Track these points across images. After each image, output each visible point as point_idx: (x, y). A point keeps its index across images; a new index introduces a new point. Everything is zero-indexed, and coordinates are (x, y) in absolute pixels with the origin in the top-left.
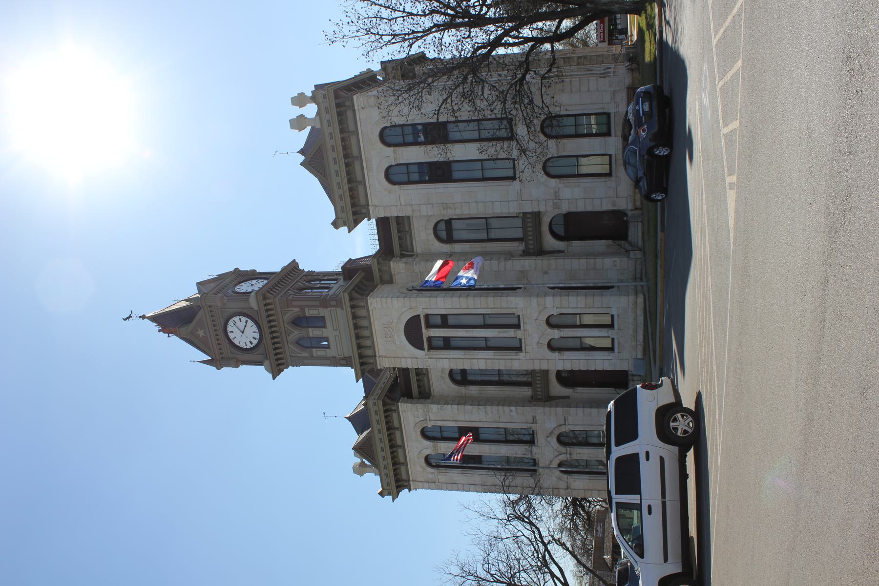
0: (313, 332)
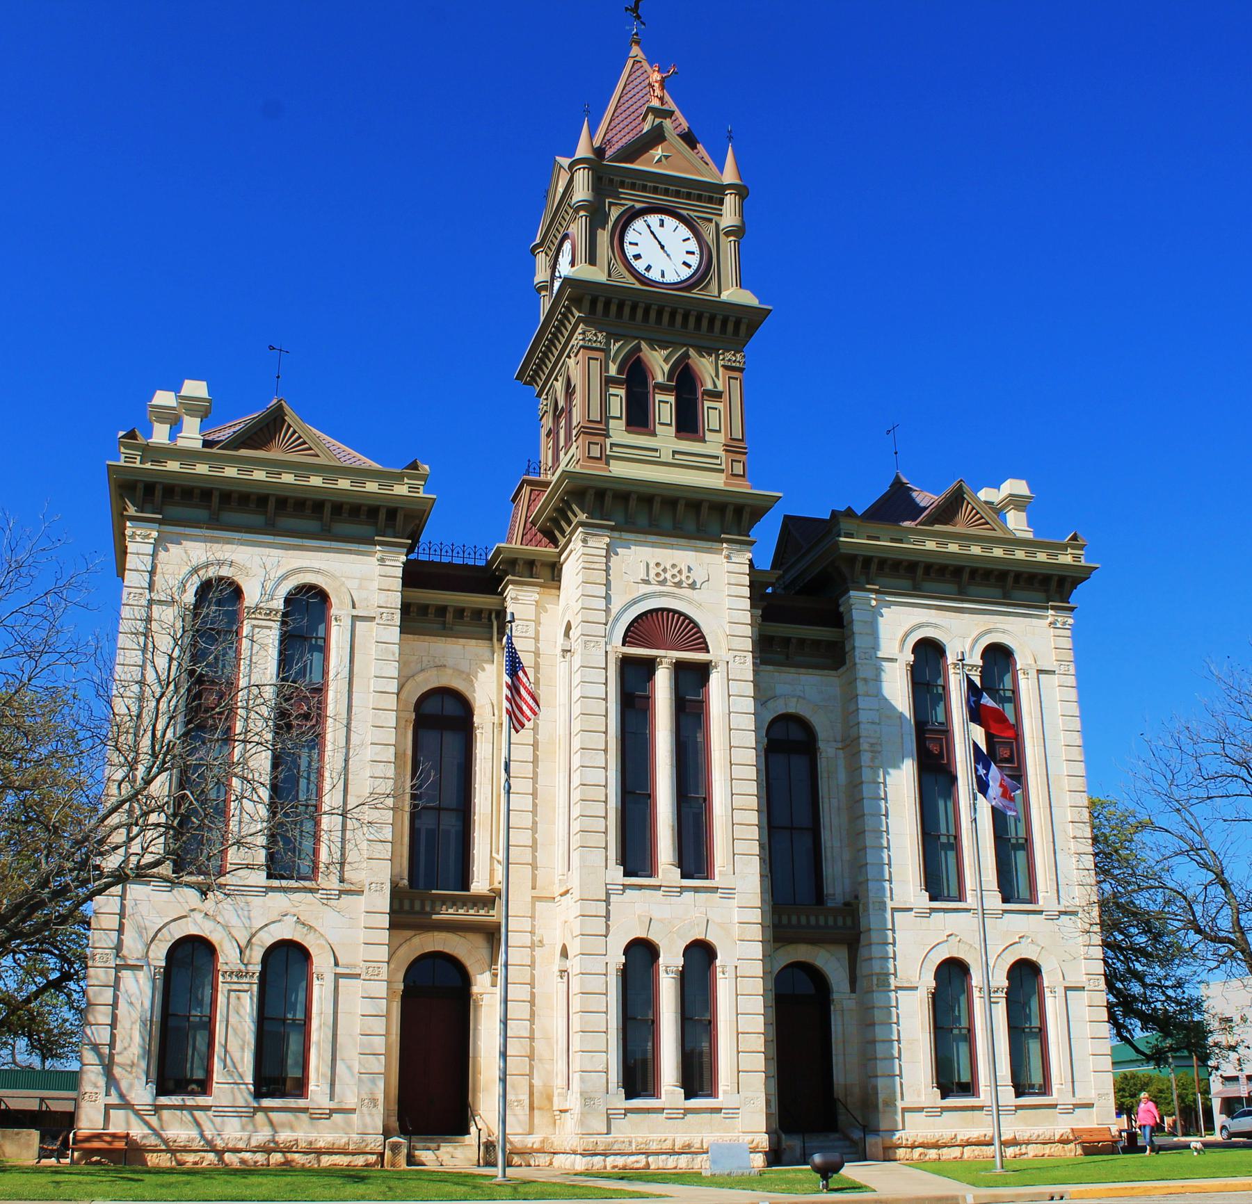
0: (664, 407)
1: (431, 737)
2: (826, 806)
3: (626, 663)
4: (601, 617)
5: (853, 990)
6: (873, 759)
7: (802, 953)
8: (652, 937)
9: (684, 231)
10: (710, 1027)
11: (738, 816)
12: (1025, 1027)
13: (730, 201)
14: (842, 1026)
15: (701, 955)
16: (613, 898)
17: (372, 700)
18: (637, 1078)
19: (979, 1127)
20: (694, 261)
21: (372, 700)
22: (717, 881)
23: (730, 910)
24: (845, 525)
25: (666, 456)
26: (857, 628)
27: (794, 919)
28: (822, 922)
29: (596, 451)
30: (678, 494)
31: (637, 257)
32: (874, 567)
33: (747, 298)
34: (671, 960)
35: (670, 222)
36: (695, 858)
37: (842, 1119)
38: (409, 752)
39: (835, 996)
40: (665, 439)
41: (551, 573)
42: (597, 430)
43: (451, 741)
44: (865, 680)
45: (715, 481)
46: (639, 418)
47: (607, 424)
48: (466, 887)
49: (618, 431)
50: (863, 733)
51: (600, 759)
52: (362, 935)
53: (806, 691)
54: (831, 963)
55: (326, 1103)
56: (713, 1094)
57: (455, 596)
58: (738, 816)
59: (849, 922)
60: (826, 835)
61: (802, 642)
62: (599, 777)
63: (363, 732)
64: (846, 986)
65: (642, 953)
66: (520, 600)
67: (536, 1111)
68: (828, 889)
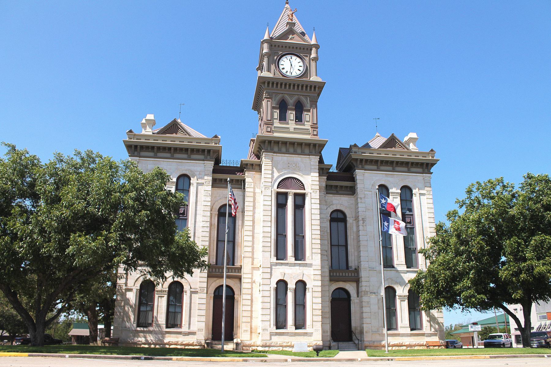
1: (334, 224)
2: (240, 234)
3: (278, 194)
4: (270, 180)
5: (358, 296)
6: (363, 223)
7: (341, 285)
8: (304, 279)
9: (298, 60)
10: (304, 306)
11: (314, 241)
12: (300, 305)
13: (314, 50)
14: (354, 308)
15: (301, 285)
16: (273, 267)
17: (203, 208)
18: (280, 324)
19: (424, 340)
20: (301, 69)
21: (203, 208)
22: (307, 261)
23: (312, 271)
24: (354, 150)
25: (292, 130)
26: (358, 181)
27: (347, 275)
28: (338, 275)
29: (269, 129)
30: (287, 140)
31: (283, 69)
32: (364, 162)
33: (319, 79)
34: (291, 285)
35: (294, 58)
36: (299, 254)
37: (354, 337)
38: (216, 224)
39: (352, 298)
40: (292, 125)
41: (258, 168)
42: (269, 123)
43: (341, 225)
44: (361, 198)
45: (308, 137)
47: (273, 121)
48: (233, 265)
49: (277, 123)
50: (360, 215)
51: (269, 224)
52: (199, 279)
53: (341, 202)
54: (350, 287)
55: (187, 330)
56: (396, 329)
57: (228, 176)
58: (314, 241)
59: (356, 275)
60: (349, 247)
61: (342, 187)
62: (268, 229)
63: (199, 218)
64: (355, 295)
65: (282, 284)
66: (249, 177)
67: (253, 334)
68: (350, 264)
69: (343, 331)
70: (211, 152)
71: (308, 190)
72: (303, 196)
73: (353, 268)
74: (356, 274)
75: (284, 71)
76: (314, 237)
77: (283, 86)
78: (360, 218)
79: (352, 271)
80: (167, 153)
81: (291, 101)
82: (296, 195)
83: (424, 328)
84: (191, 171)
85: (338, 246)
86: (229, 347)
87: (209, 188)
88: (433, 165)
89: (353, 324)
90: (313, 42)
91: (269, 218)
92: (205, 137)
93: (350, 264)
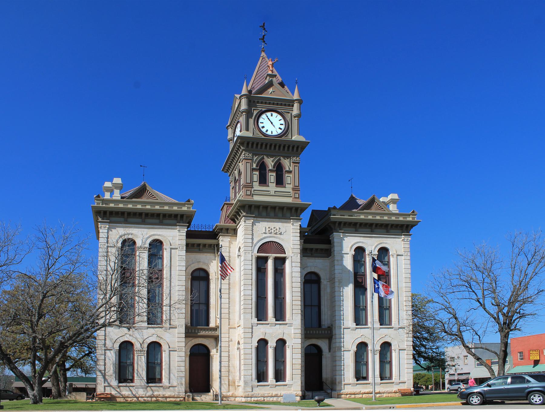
0: (272, 177)
3: (258, 258)
5: (330, 351)
8: (266, 338)
9: (280, 117)
13: (296, 105)
18: (261, 376)
20: (283, 127)
22: (287, 321)
23: (291, 330)
24: (333, 212)
26: (335, 244)
30: (276, 205)
31: (263, 127)
32: (342, 225)
33: (301, 139)
34: (272, 344)
35: (275, 114)
36: (280, 315)
37: (325, 387)
38: (190, 287)
40: (272, 187)
42: (248, 186)
43: (315, 286)
44: (338, 260)
45: (289, 200)
46: (263, 181)
47: (252, 184)
48: (208, 326)
49: (256, 186)
50: (336, 276)
53: (318, 265)
54: (323, 344)
55: (168, 385)
57: (202, 240)
61: (317, 249)
63: (175, 282)
64: (327, 350)
65: (263, 343)
66: (224, 241)
69: (318, 382)
70: (185, 217)
71: (289, 253)
72: (283, 260)
73: (326, 326)
74: (329, 332)
75: (264, 130)
76: (294, 298)
77: (286, 148)
78: (336, 280)
79: (325, 329)
80: (120, 217)
81: (270, 163)
82: (276, 259)
83: (394, 378)
84: (164, 237)
85: (311, 306)
86: (207, 398)
87: (184, 253)
88: (412, 226)
89: (324, 375)
90: (296, 96)
91: (249, 282)
92: (177, 201)
93: (323, 323)
